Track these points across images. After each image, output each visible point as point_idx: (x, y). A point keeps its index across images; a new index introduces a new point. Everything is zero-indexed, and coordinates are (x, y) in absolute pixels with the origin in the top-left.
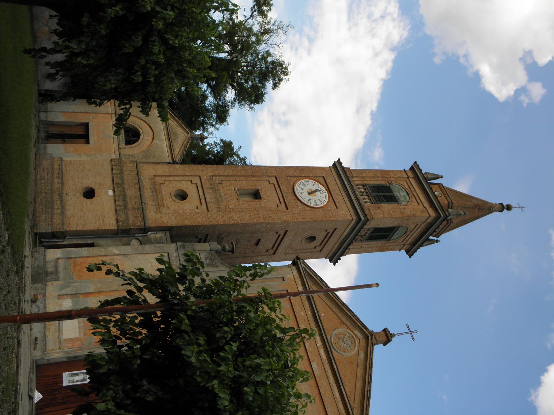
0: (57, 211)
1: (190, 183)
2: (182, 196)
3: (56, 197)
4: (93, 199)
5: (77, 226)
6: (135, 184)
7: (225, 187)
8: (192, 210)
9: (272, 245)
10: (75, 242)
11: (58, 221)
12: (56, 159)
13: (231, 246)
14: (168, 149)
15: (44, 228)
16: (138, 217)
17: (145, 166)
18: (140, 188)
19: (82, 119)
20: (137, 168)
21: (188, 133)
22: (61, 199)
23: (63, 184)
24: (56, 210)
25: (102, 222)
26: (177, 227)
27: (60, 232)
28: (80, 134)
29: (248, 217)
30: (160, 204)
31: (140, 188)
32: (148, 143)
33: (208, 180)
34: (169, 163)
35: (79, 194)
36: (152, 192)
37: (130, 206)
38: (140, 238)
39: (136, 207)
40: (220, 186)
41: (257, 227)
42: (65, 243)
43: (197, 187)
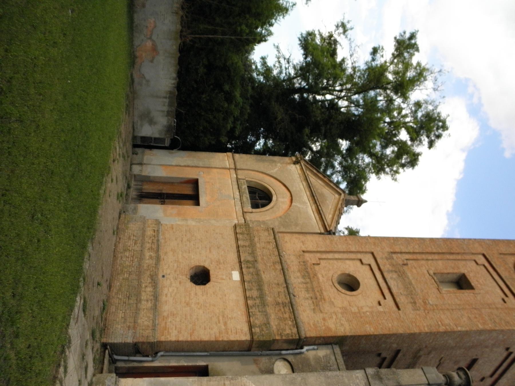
0: (146, 305)
1: (358, 263)
2: (351, 284)
3: (146, 280)
4: (208, 285)
5: (179, 332)
6: (274, 263)
7: (414, 271)
8: (372, 307)
9: (492, 369)
10: (173, 363)
11: (146, 323)
12: (150, 222)
13: (463, 377)
14: (316, 215)
15: (121, 334)
16: (285, 319)
17: (287, 237)
18: (283, 269)
19: (190, 174)
20: (275, 238)
21: (340, 194)
22: (155, 284)
23: (158, 259)
24: (143, 302)
25: (223, 327)
26: (353, 337)
27: (149, 343)
28: (189, 193)
29: (465, 319)
30: (319, 297)
31: (283, 269)
32: (286, 206)
33: (387, 259)
34: (321, 234)
35: (184, 277)
36: (303, 277)
37: (269, 299)
38: (290, 358)
39: (280, 301)
40: (405, 268)
41: (482, 338)
42: (156, 364)
43: (372, 269)
